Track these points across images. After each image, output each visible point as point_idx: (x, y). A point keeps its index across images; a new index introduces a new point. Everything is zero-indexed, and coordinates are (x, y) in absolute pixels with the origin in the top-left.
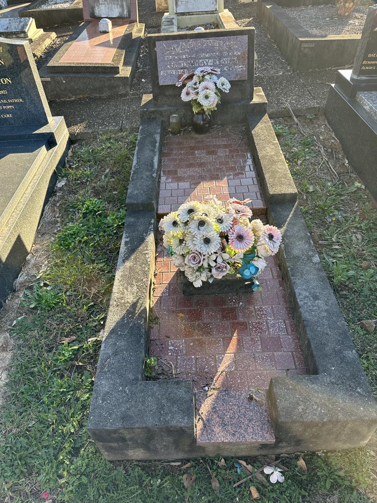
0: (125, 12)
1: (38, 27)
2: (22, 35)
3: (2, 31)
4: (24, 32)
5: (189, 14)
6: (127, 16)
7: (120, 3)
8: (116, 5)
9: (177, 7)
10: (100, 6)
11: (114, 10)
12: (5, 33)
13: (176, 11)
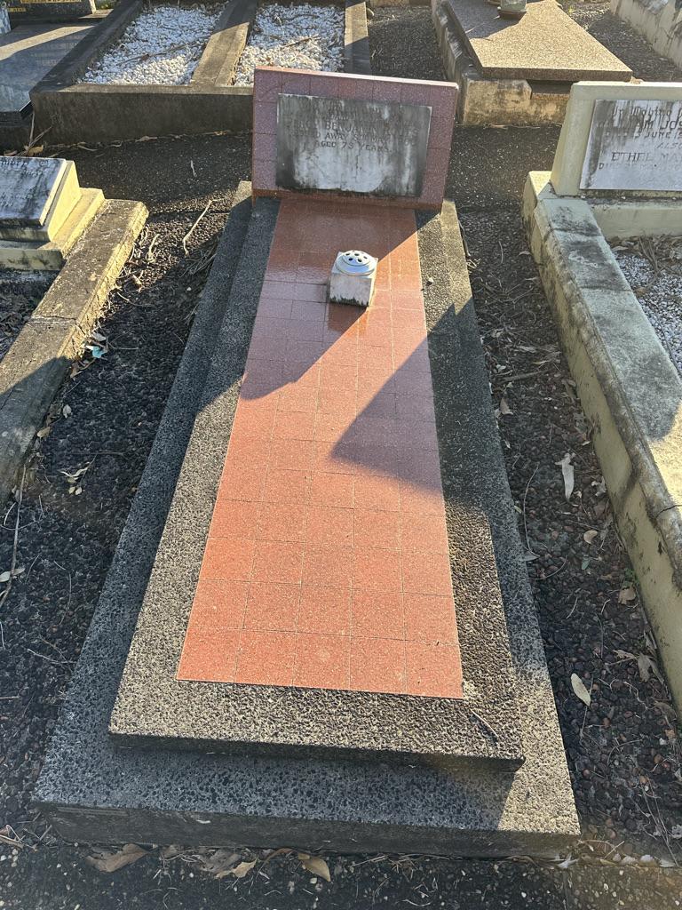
0: (407, 178)
1: (84, 181)
2: (28, 233)
3: (2, 215)
4: (36, 225)
5: (630, 196)
6: (411, 190)
7: (390, 146)
8: (375, 154)
9: (593, 169)
10: (319, 151)
11: (366, 167)
13: (588, 185)
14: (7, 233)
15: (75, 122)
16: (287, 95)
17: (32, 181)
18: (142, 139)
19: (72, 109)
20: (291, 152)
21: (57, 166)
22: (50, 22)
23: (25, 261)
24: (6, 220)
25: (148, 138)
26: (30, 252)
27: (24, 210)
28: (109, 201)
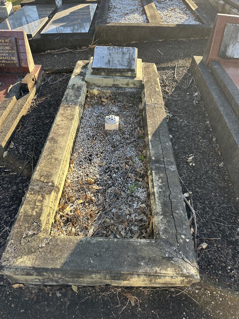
2: (129, 74)
12: (107, 69)
14: (122, 74)
15: (109, 36)
16: (230, 24)
17: (127, 55)
18: (133, 42)
19: (110, 31)
20: (227, 45)
21: (134, 50)
22: (75, 2)
23: (128, 84)
24: (122, 69)
25: (134, 42)
26: (131, 81)
27: (128, 66)
28: (144, 63)
